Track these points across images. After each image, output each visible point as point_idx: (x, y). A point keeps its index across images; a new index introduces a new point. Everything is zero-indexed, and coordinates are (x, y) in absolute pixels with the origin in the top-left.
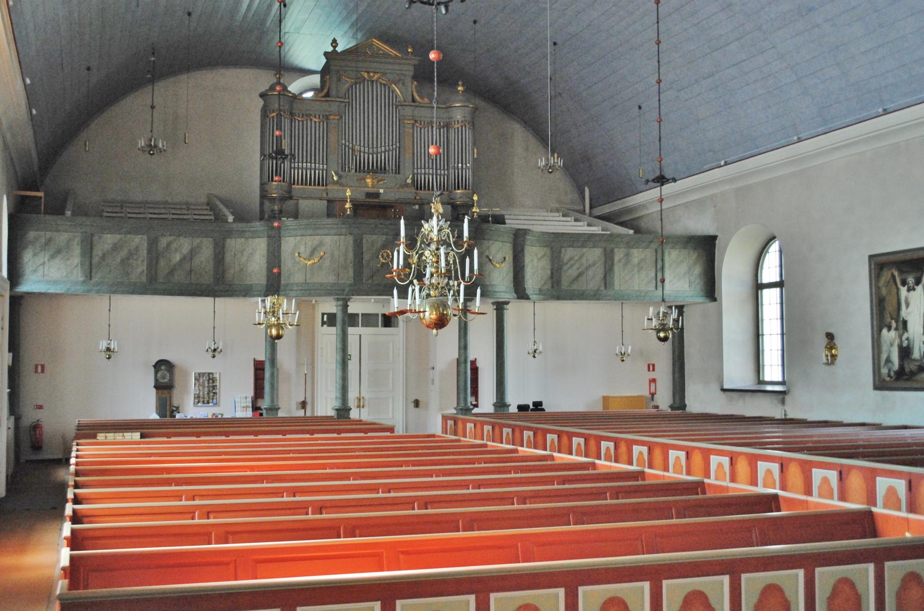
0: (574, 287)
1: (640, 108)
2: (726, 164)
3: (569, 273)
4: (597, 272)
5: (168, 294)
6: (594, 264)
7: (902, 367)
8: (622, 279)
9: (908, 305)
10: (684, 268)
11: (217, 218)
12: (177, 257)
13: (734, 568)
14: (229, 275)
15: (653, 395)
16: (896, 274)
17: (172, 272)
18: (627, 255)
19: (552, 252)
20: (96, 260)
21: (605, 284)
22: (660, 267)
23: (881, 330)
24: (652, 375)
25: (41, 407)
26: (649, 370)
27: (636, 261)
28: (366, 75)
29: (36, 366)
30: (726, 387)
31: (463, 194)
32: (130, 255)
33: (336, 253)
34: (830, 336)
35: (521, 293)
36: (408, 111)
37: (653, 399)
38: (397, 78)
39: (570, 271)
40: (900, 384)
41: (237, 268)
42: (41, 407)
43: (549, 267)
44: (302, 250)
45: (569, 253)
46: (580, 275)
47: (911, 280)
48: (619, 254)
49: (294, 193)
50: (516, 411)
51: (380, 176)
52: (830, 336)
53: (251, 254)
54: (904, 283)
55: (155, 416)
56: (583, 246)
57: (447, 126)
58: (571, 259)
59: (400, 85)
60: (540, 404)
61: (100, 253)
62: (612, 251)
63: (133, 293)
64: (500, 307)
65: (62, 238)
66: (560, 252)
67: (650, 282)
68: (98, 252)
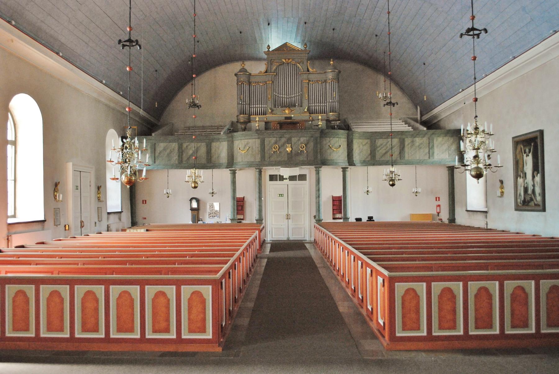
0: (383, 159)
1: (424, 64)
2: (463, 90)
3: (380, 152)
7: (525, 198)
8: (409, 154)
9: (526, 164)
10: (445, 147)
11: (208, 134)
12: (191, 152)
13: (142, 283)
14: (213, 159)
15: (438, 213)
16: (522, 147)
17: (188, 159)
18: (413, 142)
19: (371, 142)
20: (157, 154)
21: (400, 156)
22: (431, 147)
23: (517, 178)
25: (145, 218)
27: (417, 144)
28: (284, 60)
29: (143, 201)
30: (468, 209)
31: (333, 115)
32: (171, 152)
33: (254, 147)
34: (502, 182)
35: (351, 162)
36: (305, 76)
37: (438, 215)
38: (300, 60)
39: (380, 151)
40: (524, 208)
41: (217, 155)
42: (145, 218)
44: (240, 146)
45: (379, 142)
46: (386, 153)
47: (527, 150)
48: (408, 141)
49: (251, 119)
50: (355, 221)
51: (292, 109)
52: (502, 182)
53: (221, 149)
54: (525, 153)
55: (191, 222)
57: (325, 81)
58: (382, 144)
59: (301, 64)
60: (372, 217)
61: (159, 152)
62: (404, 140)
63: (180, 168)
64: (344, 170)
66: (375, 141)
67: (426, 154)
68: (158, 151)
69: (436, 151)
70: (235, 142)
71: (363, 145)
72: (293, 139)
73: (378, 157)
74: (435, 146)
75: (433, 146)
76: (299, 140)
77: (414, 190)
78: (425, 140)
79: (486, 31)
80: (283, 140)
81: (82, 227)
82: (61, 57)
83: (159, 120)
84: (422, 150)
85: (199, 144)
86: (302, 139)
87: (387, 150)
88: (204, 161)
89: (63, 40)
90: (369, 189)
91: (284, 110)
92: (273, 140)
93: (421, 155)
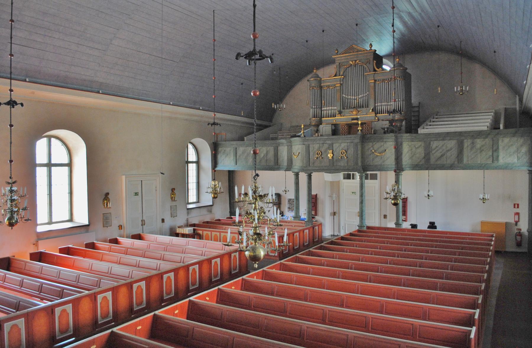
0: (439, 162)
3: (435, 155)
4: (454, 153)
5: (271, 170)
6: (451, 149)
12: (262, 155)
14: (279, 162)
15: (516, 223)
20: (237, 157)
22: (495, 150)
24: (517, 210)
26: (515, 207)
27: (478, 146)
37: (516, 225)
43: (423, 152)
45: (434, 144)
46: (442, 156)
51: (359, 109)
56: (443, 140)
59: (368, 64)
65: (228, 149)
66: (430, 144)
67: (489, 157)
69: (502, 154)
70: (293, 147)
71: (416, 148)
72: (334, 145)
73: (432, 161)
74: (500, 147)
75: (498, 148)
76: (340, 145)
77: (481, 196)
78: (488, 141)
79: (22, 105)
80: (326, 146)
81: (143, 225)
82: (102, 94)
83: (271, 121)
84: (484, 153)
85: (268, 148)
86: (343, 145)
87: (443, 152)
88: (272, 163)
89: (101, 80)
90: (430, 193)
91: (352, 112)
92: (317, 146)
93: (483, 158)
